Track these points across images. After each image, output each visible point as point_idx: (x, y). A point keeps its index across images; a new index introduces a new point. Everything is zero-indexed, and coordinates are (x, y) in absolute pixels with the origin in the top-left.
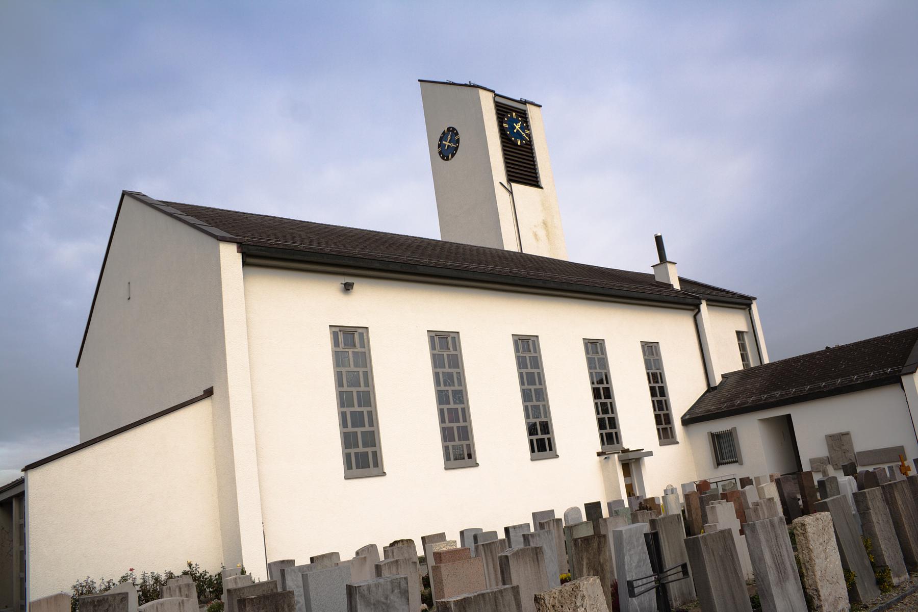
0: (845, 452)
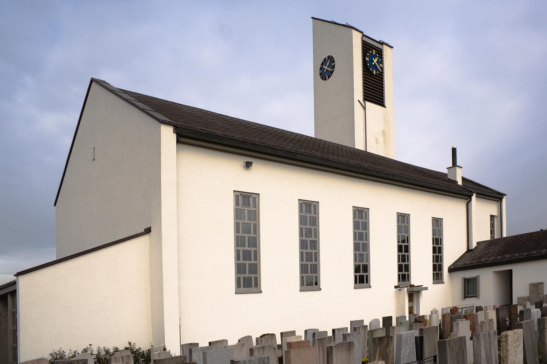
0: (538, 294)
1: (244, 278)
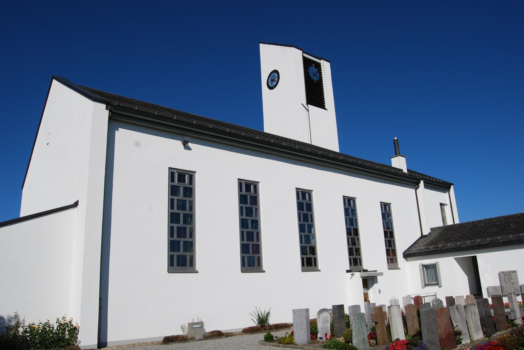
0: (513, 284)
1: (178, 256)
